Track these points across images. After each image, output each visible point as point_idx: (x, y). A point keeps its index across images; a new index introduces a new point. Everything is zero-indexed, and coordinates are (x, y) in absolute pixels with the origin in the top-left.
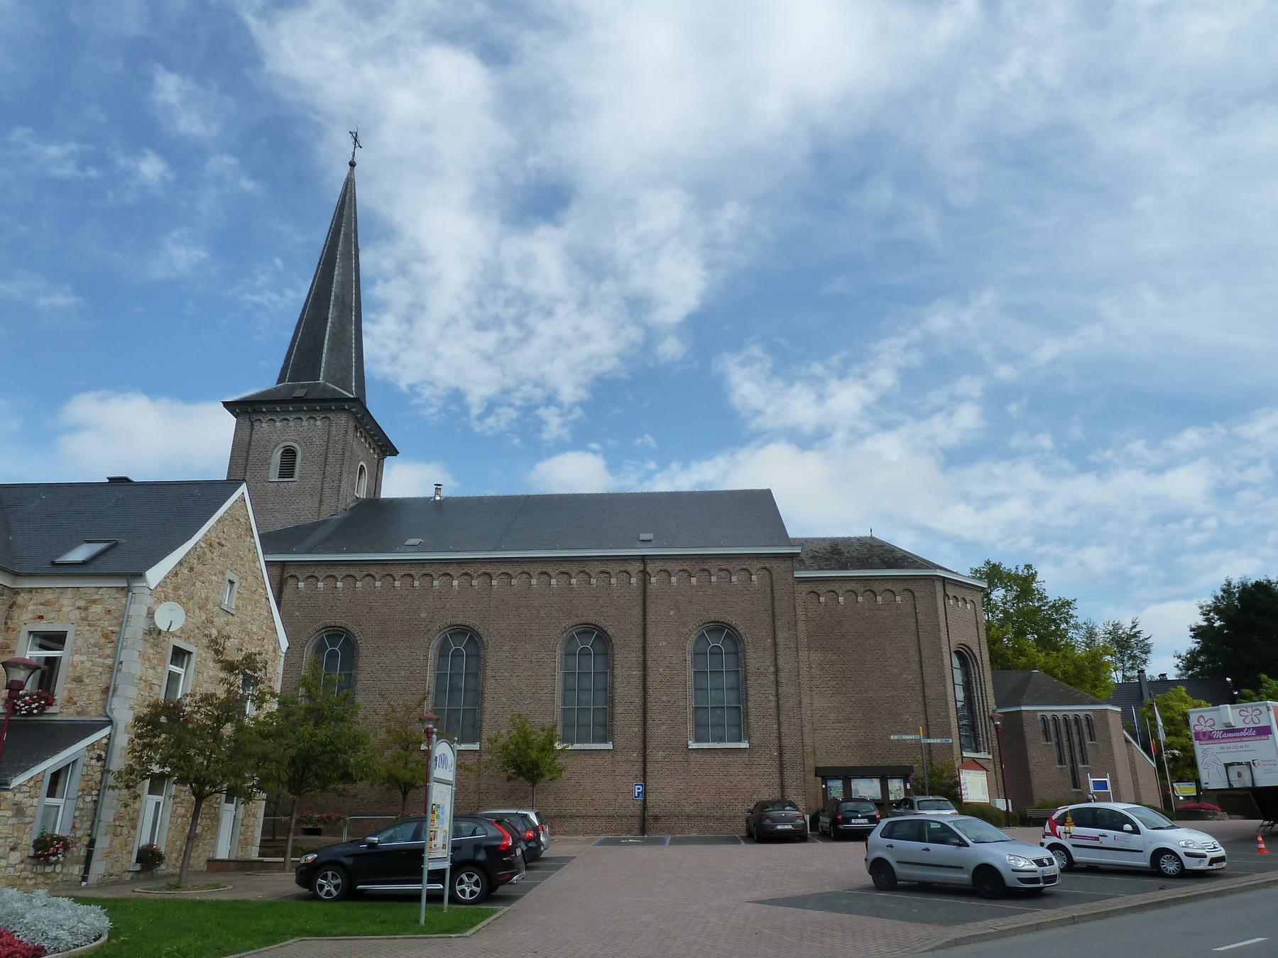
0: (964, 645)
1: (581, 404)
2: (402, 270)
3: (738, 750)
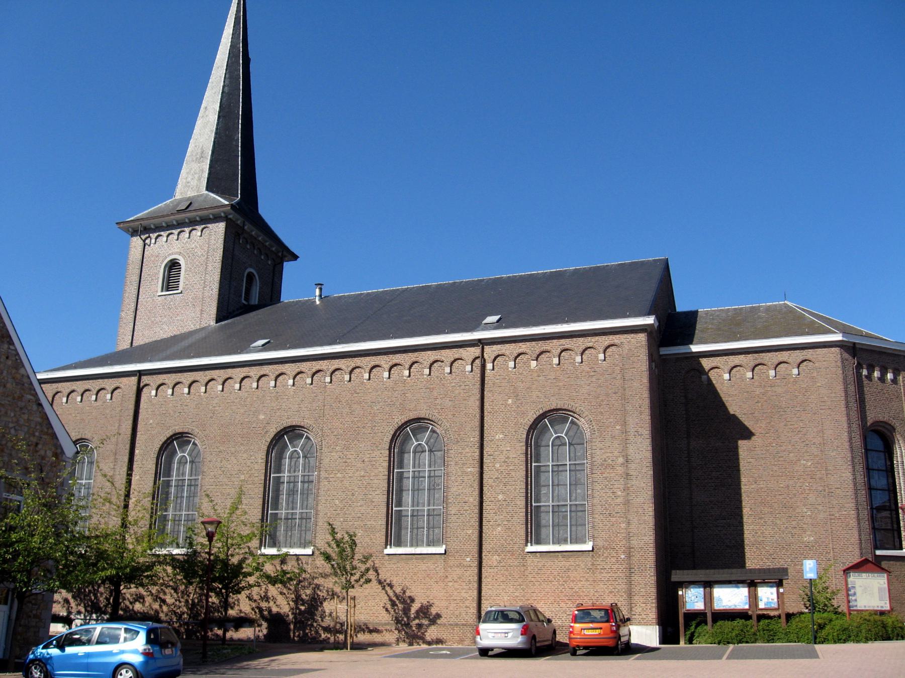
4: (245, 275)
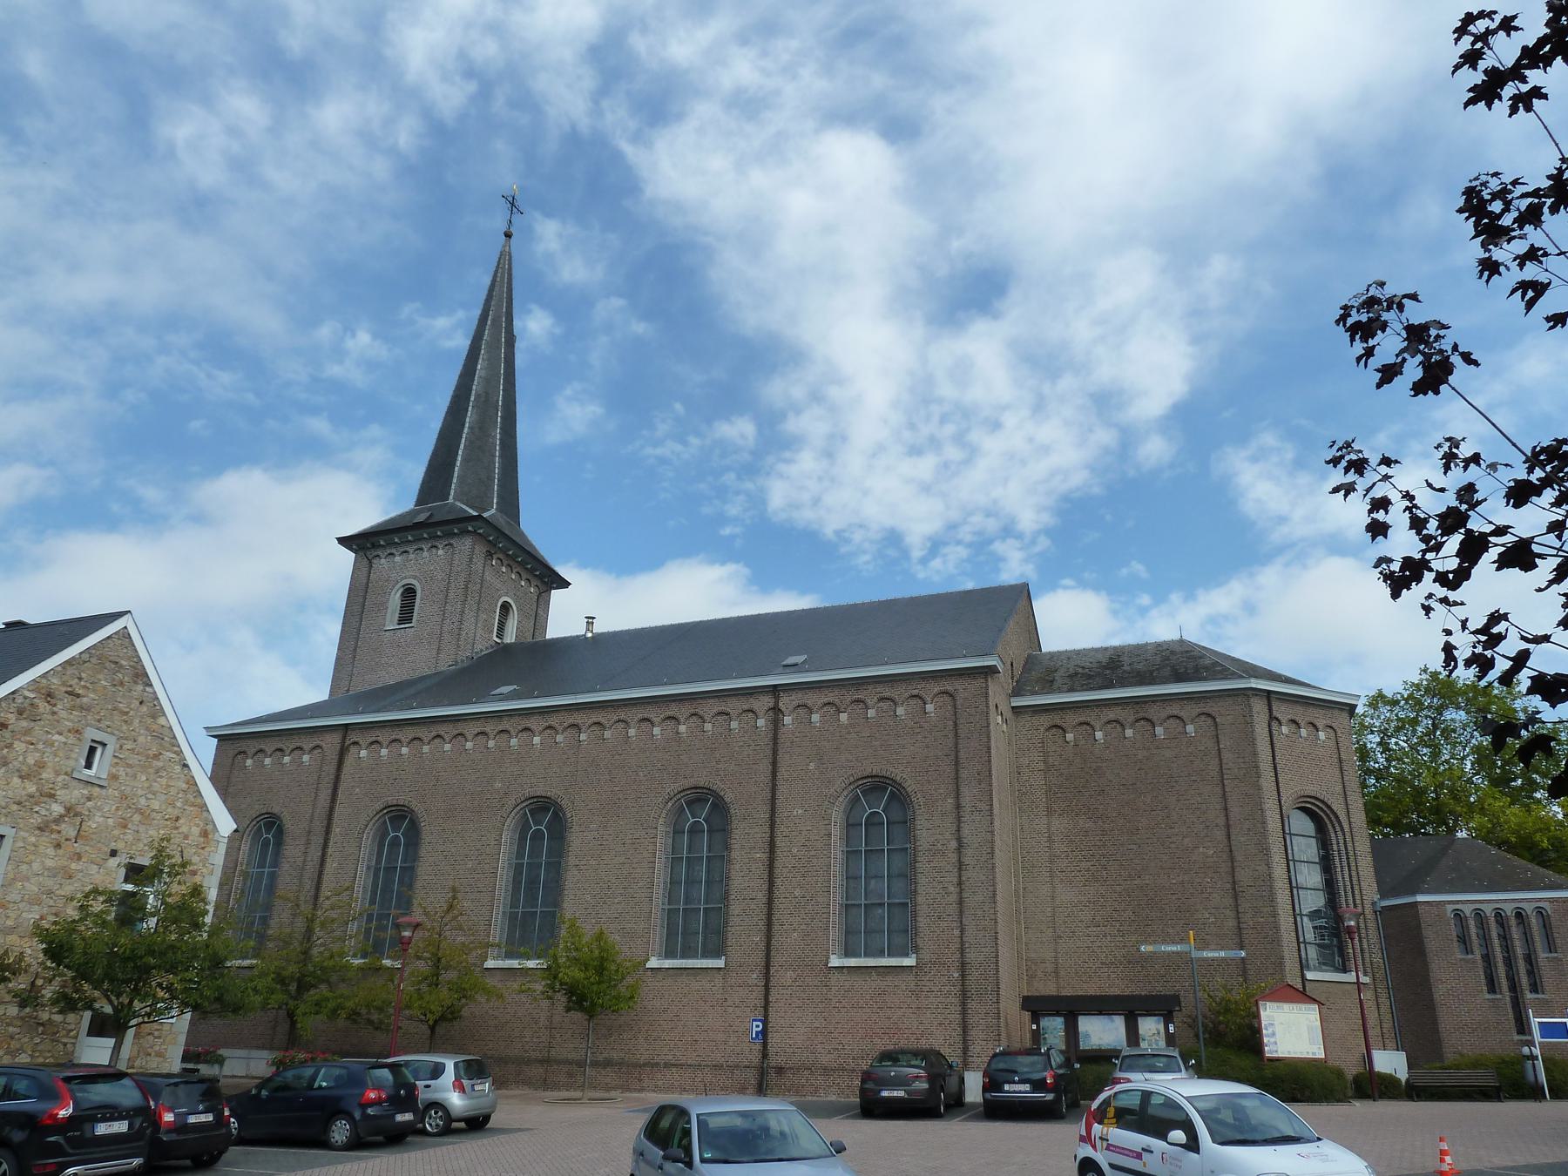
1: (1048, 532)
2: (816, 397)
3: (899, 969)
4: (499, 605)
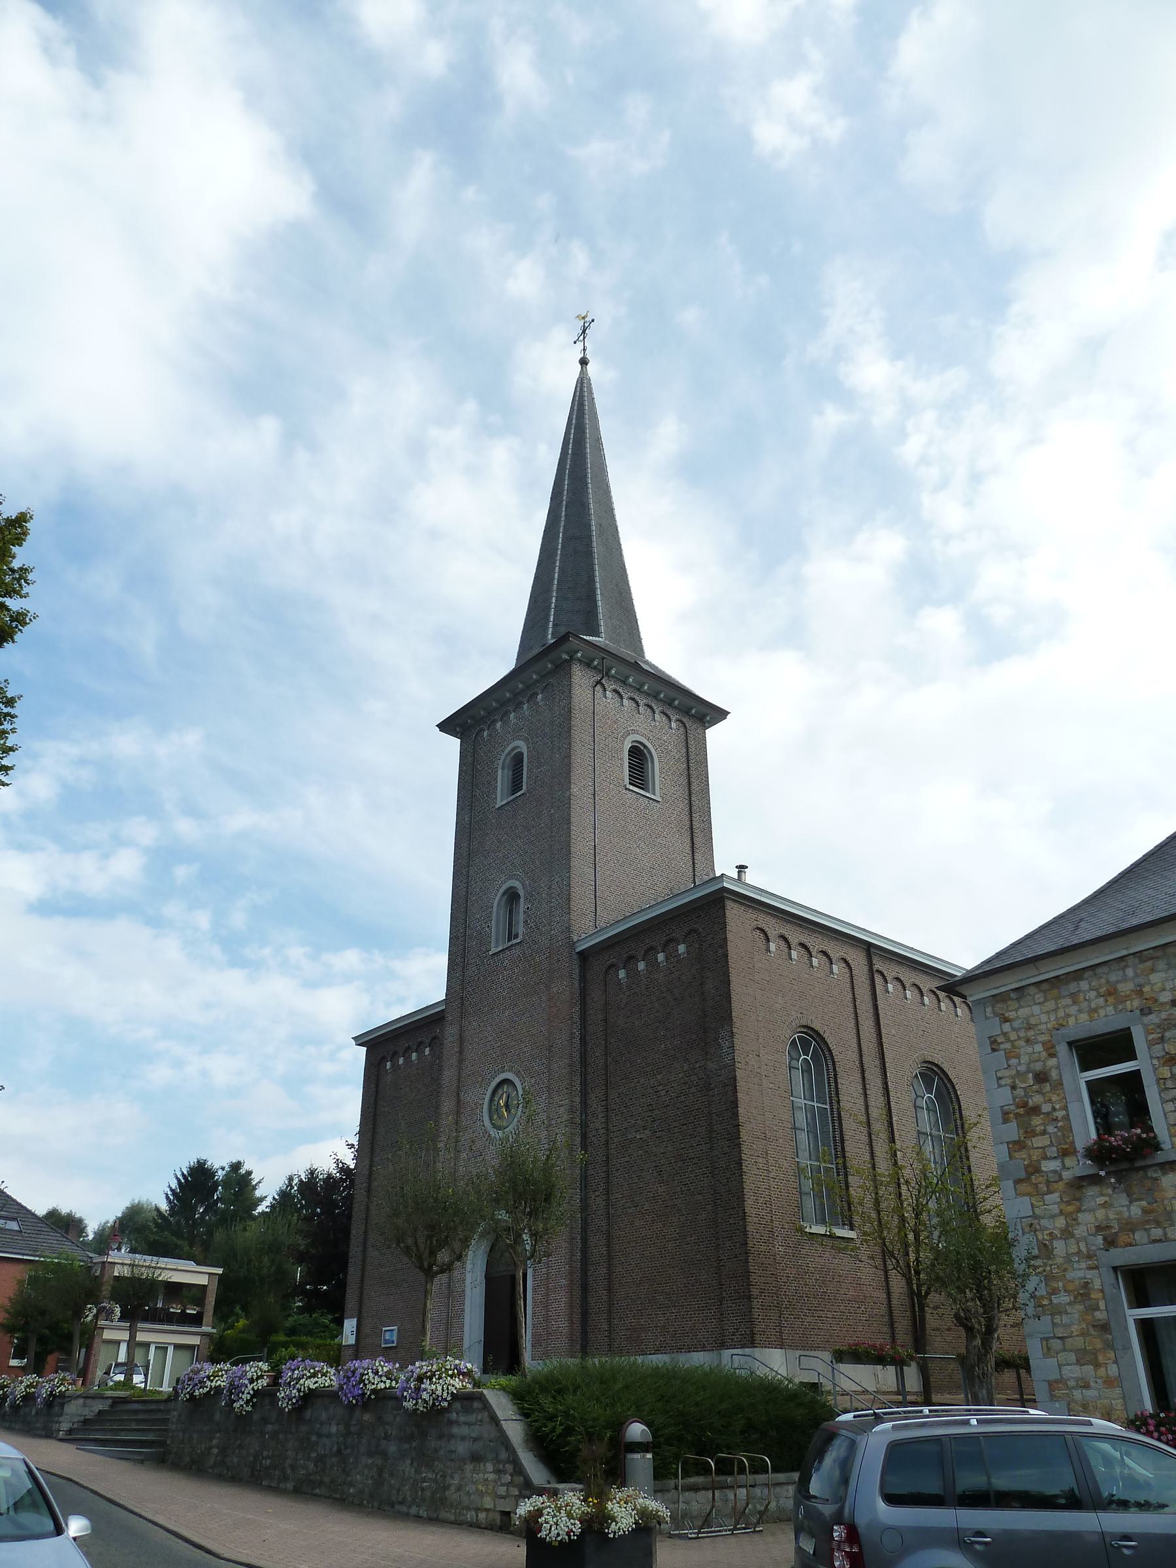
0: (937, 1065)
